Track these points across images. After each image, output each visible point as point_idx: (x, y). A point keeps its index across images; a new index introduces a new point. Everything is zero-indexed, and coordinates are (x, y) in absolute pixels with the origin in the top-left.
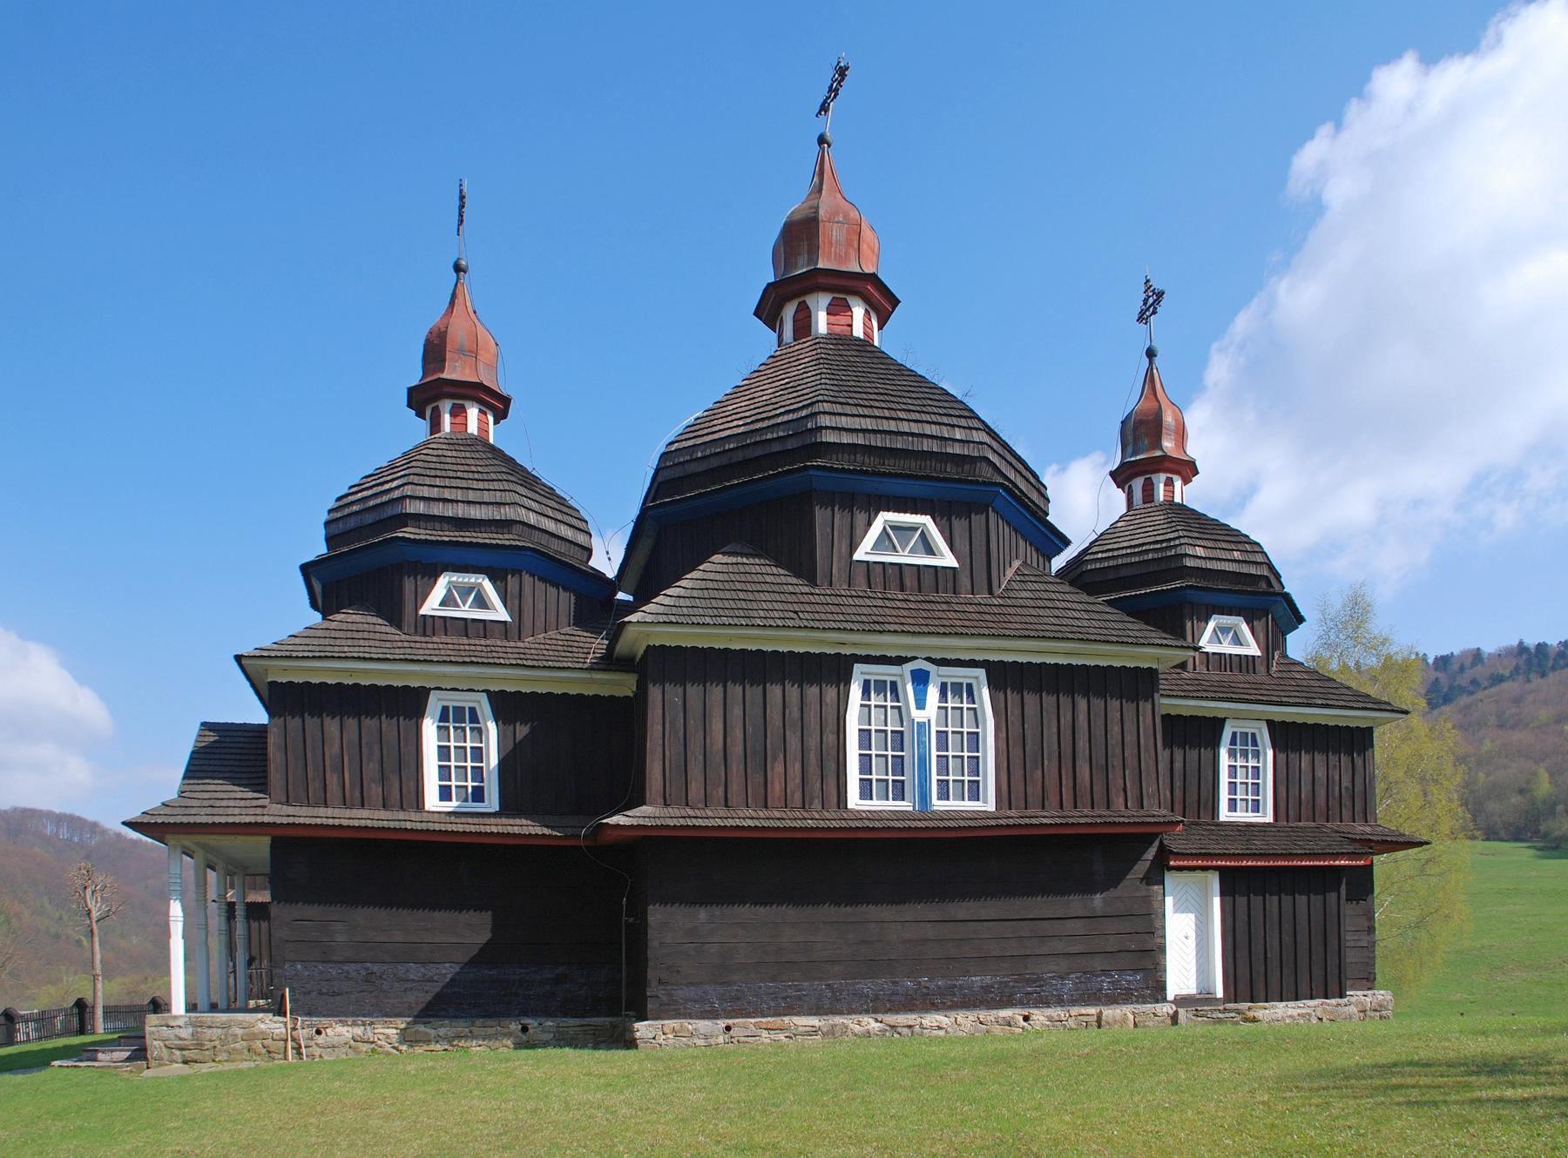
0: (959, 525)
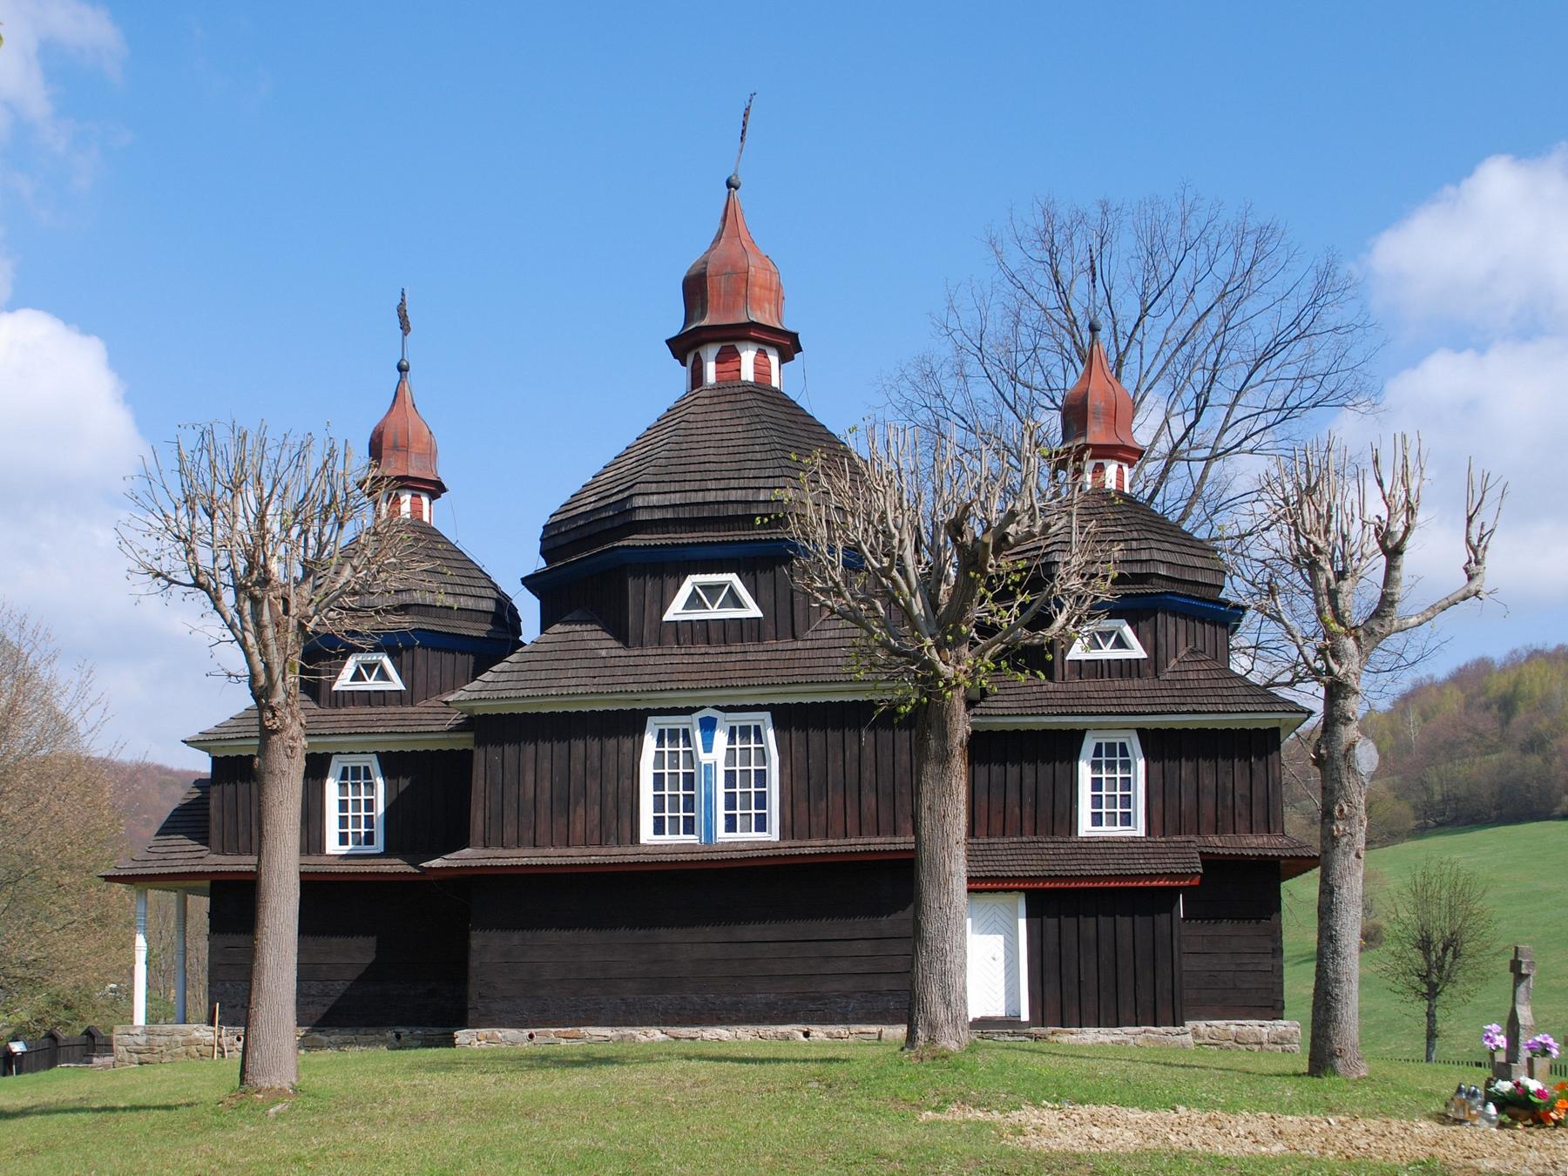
0: (764, 578)
